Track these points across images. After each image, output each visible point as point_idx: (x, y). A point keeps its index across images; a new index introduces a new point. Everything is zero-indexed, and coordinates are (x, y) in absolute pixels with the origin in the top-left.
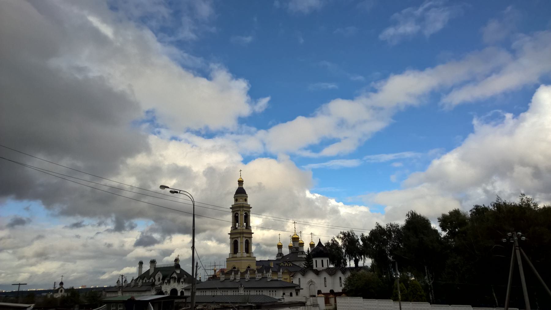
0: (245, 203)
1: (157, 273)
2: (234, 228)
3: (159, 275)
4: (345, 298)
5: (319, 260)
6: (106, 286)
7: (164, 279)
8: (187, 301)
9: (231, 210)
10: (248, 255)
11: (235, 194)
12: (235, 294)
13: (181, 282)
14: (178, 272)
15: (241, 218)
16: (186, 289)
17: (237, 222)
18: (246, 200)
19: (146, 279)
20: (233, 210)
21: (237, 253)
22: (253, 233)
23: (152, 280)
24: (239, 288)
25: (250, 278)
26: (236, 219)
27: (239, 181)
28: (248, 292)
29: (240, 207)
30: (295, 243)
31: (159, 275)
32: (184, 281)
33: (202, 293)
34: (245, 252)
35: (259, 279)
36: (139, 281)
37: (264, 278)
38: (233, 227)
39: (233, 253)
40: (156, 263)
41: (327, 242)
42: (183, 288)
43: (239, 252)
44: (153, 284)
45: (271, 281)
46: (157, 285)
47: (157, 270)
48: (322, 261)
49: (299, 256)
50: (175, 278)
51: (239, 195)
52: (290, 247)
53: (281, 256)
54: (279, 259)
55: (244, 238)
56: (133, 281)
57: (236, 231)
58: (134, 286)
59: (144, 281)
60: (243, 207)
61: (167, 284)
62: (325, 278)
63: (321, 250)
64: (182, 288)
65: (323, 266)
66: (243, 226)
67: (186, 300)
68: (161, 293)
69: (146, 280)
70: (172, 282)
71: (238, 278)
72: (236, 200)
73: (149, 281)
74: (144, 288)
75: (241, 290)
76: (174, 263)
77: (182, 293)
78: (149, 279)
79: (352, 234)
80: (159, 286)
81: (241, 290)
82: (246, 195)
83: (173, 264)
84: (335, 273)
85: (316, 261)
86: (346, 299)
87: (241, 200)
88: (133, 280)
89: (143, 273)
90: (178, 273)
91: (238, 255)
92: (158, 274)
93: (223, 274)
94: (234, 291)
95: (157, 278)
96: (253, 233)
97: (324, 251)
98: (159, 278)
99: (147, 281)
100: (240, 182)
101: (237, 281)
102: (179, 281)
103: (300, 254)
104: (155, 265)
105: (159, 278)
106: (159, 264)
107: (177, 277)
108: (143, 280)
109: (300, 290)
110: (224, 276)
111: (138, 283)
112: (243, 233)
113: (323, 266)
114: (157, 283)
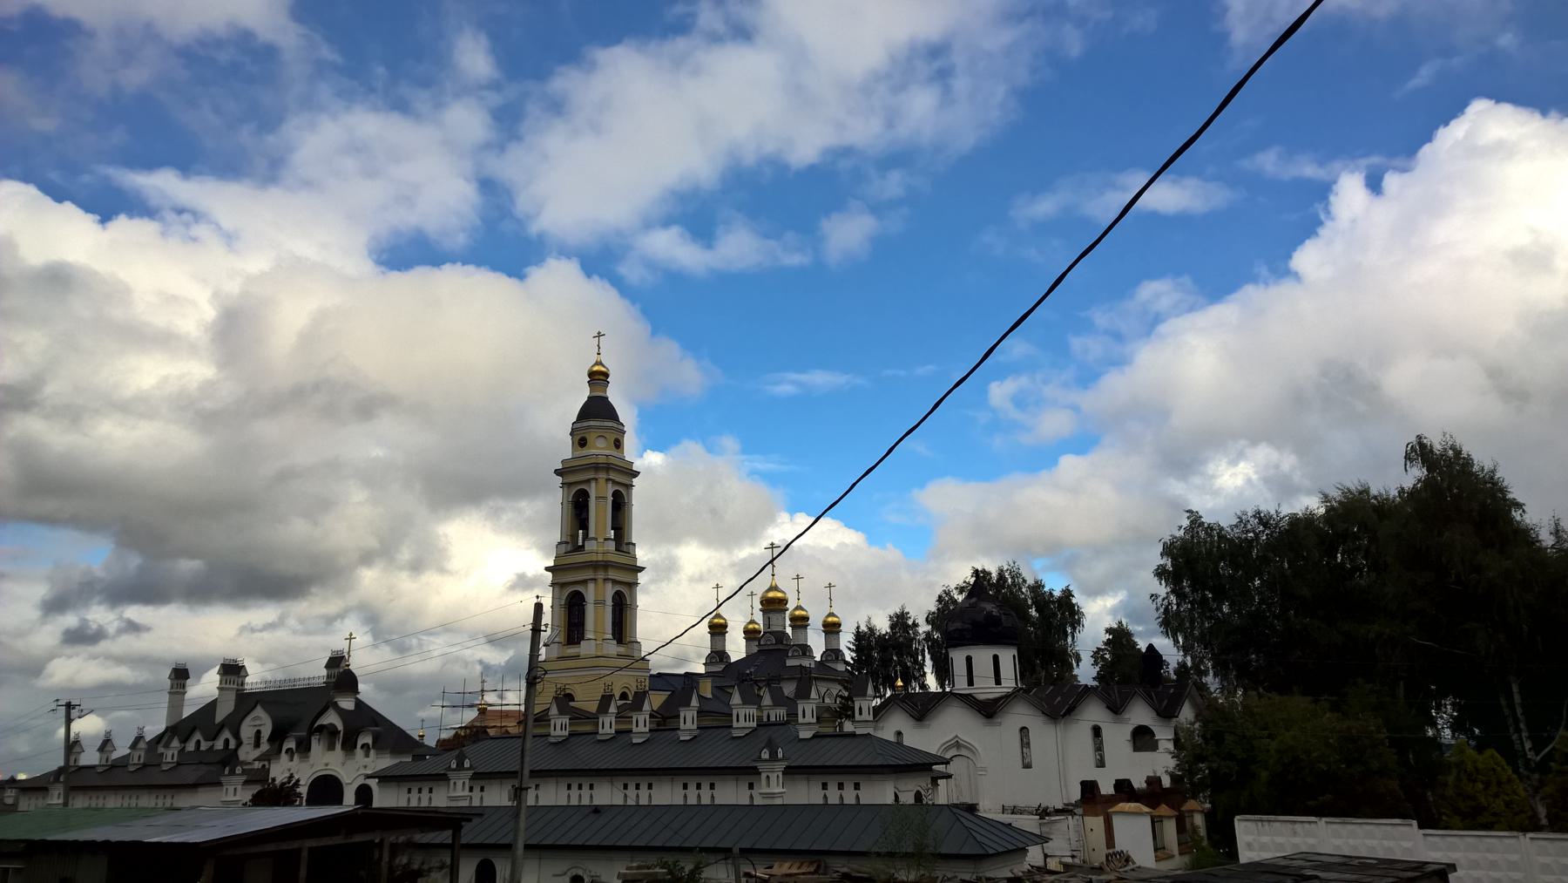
0: (615, 453)
1: (248, 713)
2: (569, 547)
3: (258, 722)
4: (1295, 822)
5: (982, 657)
7: (278, 736)
8: (464, 841)
9: (560, 479)
10: (622, 650)
12: (692, 801)
13: (359, 746)
14: (347, 704)
15: (599, 513)
16: (385, 778)
18: (618, 444)
19: (198, 736)
20: (565, 481)
23: (227, 741)
24: (450, 774)
25: (650, 730)
26: (578, 509)
27: (592, 374)
28: (644, 792)
29: (596, 467)
30: (774, 617)
31: (260, 721)
32: (374, 742)
33: (632, 792)
34: (611, 637)
35: (747, 731)
37: (765, 725)
38: (567, 543)
39: (562, 641)
41: (898, 611)
42: (369, 772)
44: (229, 759)
45: (815, 736)
46: (249, 763)
47: (247, 701)
48: (996, 658)
49: (790, 663)
50: (331, 732)
51: (592, 423)
52: (750, 634)
53: (721, 661)
55: (609, 585)
56: (142, 745)
57: (578, 558)
58: (145, 766)
59: (191, 746)
60: (608, 468)
61: (296, 756)
63: (990, 614)
64: (363, 771)
65: (998, 682)
66: (606, 539)
67: (455, 836)
68: (281, 795)
69: (198, 742)
70: (317, 746)
71: (641, 728)
72: (582, 443)
74: (190, 775)
75: (460, 783)
76: (324, 672)
77: (364, 793)
78: (215, 738)
79: (1012, 578)
80: (257, 765)
81: (460, 783)
82: (621, 427)
83: (316, 672)
85: (969, 660)
86: (1297, 826)
87: (601, 443)
88: (139, 739)
90: (343, 709)
91: (585, 648)
92: (255, 719)
93: (562, 712)
94: (569, 787)
95: (247, 731)
97: (1003, 617)
98: (259, 732)
99: (204, 746)
100: (597, 377)
101: (635, 741)
102: (349, 746)
103: (793, 657)
104: (243, 684)
105: (259, 732)
106: (256, 677)
107: (340, 727)
108: (184, 741)
110: (565, 720)
111: (163, 754)
112: (606, 566)
114: (247, 753)
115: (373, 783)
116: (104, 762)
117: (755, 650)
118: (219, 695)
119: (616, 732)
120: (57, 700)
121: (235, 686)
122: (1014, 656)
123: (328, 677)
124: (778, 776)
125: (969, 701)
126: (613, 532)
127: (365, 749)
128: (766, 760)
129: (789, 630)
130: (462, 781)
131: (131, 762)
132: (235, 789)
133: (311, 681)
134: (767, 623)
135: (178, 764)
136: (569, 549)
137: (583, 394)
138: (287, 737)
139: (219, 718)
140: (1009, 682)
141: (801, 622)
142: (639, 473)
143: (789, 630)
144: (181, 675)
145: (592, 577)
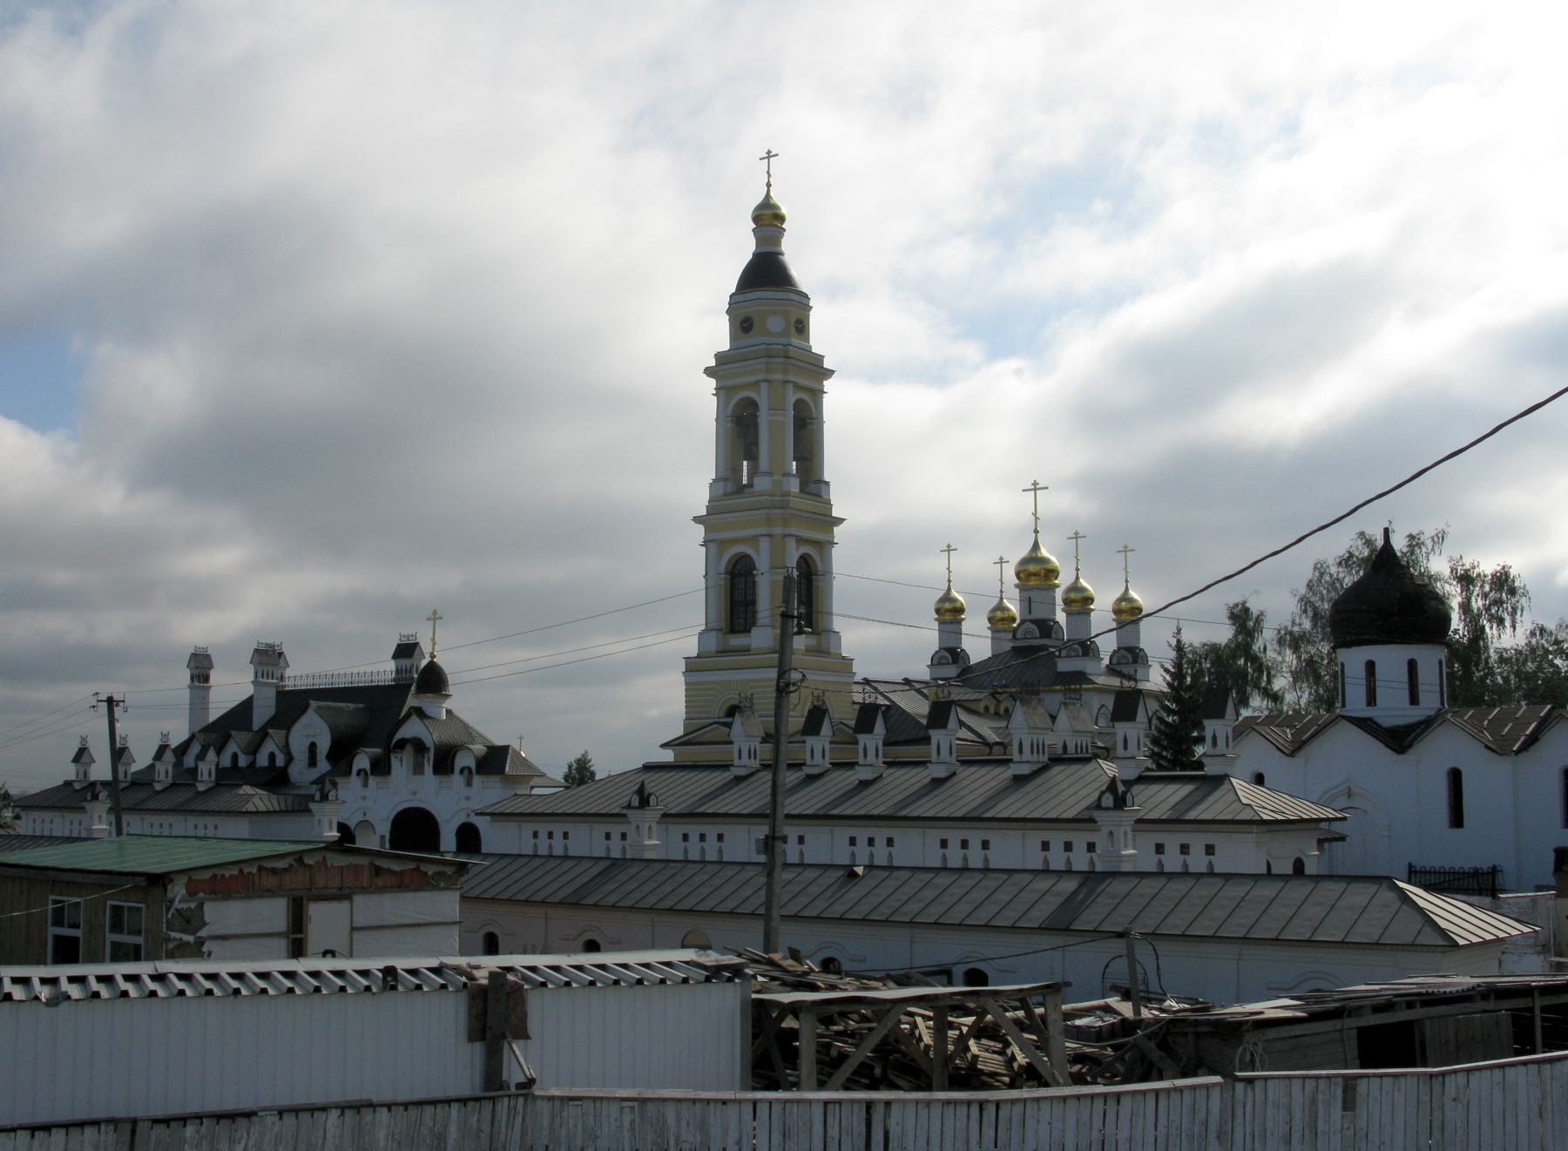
2: (730, 487)
6: (524, 755)
7: (342, 752)
11: (733, 290)
15: (774, 429)
17: (752, 455)
18: (802, 327)
21: (754, 630)
22: (841, 521)
23: (272, 757)
31: (313, 730)
36: (201, 756)
40: (285, 668)
43: (760, 622)
47: (292, 704)
48: (1412, 665)
52: (999, 619)
53: (955, 661)
54: (104, 947)
55: (791, 544)
59: (226, 761)
62: (1455, 777)
65: (1414, 699)
70: (401, 765)
73: (254, 762)
84: (1502, 755)
85: (1371, 666)
88: (162, 749)
89: (213, 716)
96: (841, 521)
98: (313, 746)
104: (282, 678)
105: (313, 746)
106: (301, 672)
109: (1290, 871)
113: (1414, 699)
115: (482, 823)
116: (81, 777)
117: (1008, 646)
118: (255, 690)
119: (1049, 759)
120: (97, 693)
121: (275, 681)
122: (1440, 662)
123: (398, 672)
124: (1125, 833)
125: (1366, 725)
126: (794, 463)
127: (362, 774)
128: (1108, 809)
129: (1061, 617)
130: (647, 826)
131: (156, 779)
132: (650, 827)
133: (376, 678)
134: (1027, 603)
135: (172, 785)
136: (729, 490)
137: (744, 249)
138: (357, 753)
139: (257, 723)
140: (1430, 700)
141: (1080, 603)
142: (834, 372)
143: (1061, 617)
144: (201, 667)
145: (764, 532)
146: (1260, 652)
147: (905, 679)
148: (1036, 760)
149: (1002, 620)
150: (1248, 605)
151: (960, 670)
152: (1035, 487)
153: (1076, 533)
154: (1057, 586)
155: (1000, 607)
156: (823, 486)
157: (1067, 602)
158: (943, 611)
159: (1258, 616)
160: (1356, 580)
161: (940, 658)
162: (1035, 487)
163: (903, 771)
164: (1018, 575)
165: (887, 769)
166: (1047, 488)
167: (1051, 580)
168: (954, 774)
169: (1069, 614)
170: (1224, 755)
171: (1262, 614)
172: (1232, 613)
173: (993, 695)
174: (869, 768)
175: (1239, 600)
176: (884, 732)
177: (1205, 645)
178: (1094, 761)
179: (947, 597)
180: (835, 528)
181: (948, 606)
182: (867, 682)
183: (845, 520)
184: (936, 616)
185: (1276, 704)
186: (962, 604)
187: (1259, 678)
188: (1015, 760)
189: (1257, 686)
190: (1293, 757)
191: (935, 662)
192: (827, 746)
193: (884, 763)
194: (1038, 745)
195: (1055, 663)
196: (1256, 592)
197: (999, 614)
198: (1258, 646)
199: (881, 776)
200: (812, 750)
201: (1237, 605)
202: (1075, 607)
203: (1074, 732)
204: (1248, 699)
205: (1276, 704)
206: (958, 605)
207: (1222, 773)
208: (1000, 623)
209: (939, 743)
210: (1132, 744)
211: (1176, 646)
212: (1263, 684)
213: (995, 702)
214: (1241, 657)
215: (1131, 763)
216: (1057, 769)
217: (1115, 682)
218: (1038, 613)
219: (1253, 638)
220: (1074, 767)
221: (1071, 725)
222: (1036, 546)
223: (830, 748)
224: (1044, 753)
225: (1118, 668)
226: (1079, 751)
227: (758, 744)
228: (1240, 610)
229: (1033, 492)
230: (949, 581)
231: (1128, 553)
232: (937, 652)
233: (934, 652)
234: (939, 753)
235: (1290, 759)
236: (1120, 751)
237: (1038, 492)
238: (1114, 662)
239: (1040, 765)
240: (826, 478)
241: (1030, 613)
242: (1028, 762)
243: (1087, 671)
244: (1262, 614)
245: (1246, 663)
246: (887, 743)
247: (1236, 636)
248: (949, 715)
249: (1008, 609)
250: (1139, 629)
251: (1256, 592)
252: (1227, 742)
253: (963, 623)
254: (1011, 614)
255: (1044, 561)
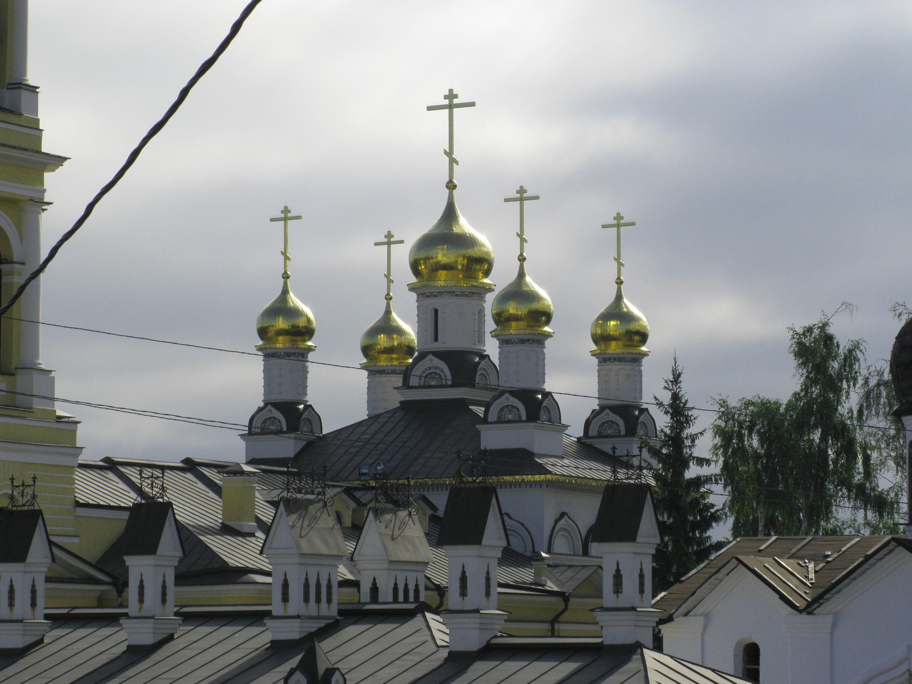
22: (59, 160)
96: (59, 160)
117: (394, 399)
119: (341, 612)
143: (492, 348)
146: (851, 418)
147: (107, 460)
148: (315, 614)
149: (389, 350)
150: (831, 330)
151: (302, 444)
152: (451, 103)
153: (522, 191)
154: (489, 289)
155: (386, 326)
156: (24, 94)
157: (501, 319)
158: (271, 334)
159: (850, 351)
160: (302, 330)
161: (265, 421)
162: (451, 103)
163: (226, 631)
164: (415, 266)
165: (52, 629)
166: (472, 104)
167: (476, 278)
168: (170, 638)
169: (505, 342)
170: (633, 609)
171: (856, 346)
172: (800, 344)
173: (349, 491)
174: (19, 626)
175: (814, 320)
176: (179, 554)
177: (748, 403)
178: (419, 617)
179: (281, 308)
180: (47, 176)
181: (281, 323)
182: (110, 465)
183: (65, 159)
184: (260, 343)
185: (881, 516)
186: (309, 320)
187: (850, 465)
188: (274, 613)
189: (845, 482)
190: (809, 613)
191: (257, 423)
192: (41, 586)
193: (47, 617)
194: (318, 586)
195: (478, 434)
196: (846, 305)
197: (382, 340)
198: (847, 406)
199: (41, 641)
200: (141, 587)
201: (810, 330)
202: (514, 329)
203: (391, 562)
204: (829, 505)
205: (881, 516)
206: (301, 323)
207: (630, 641)
208: (385, 356)
209: (142, 581)
210: (630, 583)
211: (671, 405)
212: (858, 478)
213: (353, 505)
214: (815, 427)
215: (472, 621)
216: (352, 630)
217: (601, 473)
218: (451, 341)
219: (837, 390)
220: (382, 628)
221: (385, 548)
222: (450, 214)
223: (46, 589)
224: (329, 601)
225: (605, 446)
226: (401, 598)
227: (494, 564)
228: (816, 341)
229: (446, 112)
230: (286, 277)
231: (392, 246)
232: (260, 410)
233: (255, 410)
234: (141, 600)
235: (804, 617)
236: (453, 599)
237: (455, 110)
238: (593, 431)
239: (321, 624)
240: (31, 79)
241: (436, 339)
242: (298, 617)
243: (536, 450)
244: (856, 346)
245: (823, 439)
246: (183, 578)
247: (806, 388)
248: (35, 529)
249: (400, 331)
250: (640, 372)
251: (846, 305)
252: (642, 584)
253: (548, 342)
254: (403, 340)
255: (466, 241)
